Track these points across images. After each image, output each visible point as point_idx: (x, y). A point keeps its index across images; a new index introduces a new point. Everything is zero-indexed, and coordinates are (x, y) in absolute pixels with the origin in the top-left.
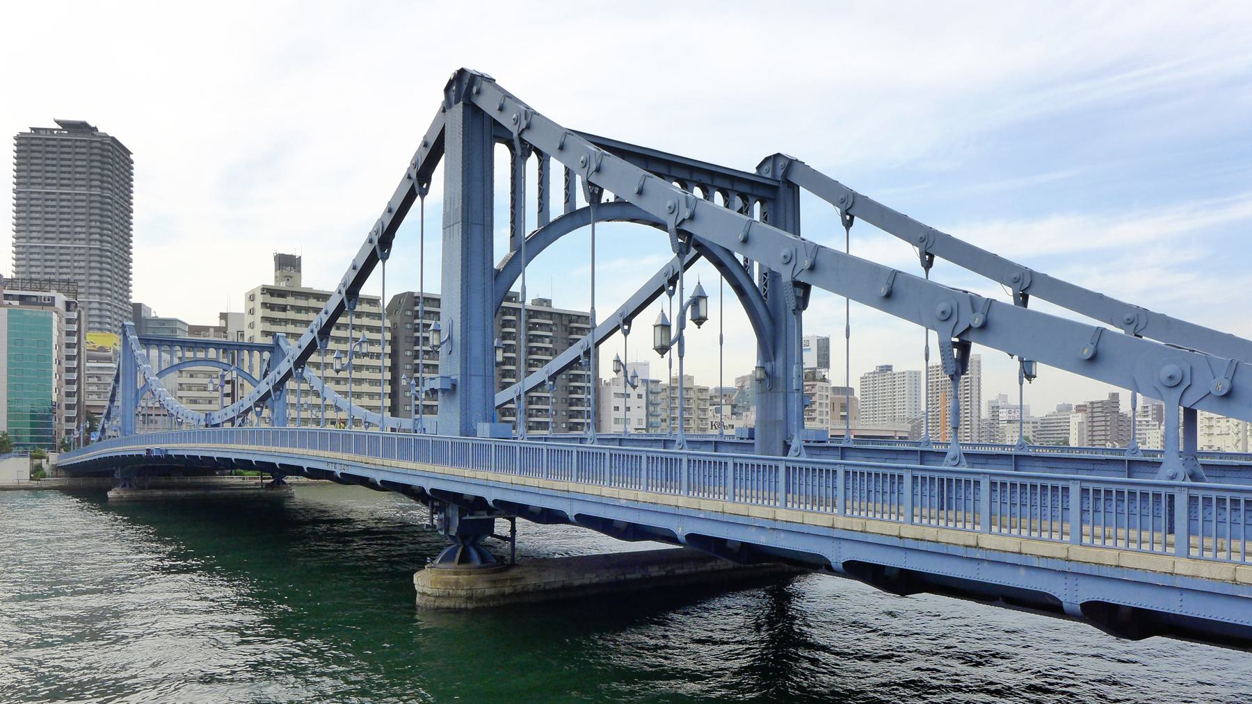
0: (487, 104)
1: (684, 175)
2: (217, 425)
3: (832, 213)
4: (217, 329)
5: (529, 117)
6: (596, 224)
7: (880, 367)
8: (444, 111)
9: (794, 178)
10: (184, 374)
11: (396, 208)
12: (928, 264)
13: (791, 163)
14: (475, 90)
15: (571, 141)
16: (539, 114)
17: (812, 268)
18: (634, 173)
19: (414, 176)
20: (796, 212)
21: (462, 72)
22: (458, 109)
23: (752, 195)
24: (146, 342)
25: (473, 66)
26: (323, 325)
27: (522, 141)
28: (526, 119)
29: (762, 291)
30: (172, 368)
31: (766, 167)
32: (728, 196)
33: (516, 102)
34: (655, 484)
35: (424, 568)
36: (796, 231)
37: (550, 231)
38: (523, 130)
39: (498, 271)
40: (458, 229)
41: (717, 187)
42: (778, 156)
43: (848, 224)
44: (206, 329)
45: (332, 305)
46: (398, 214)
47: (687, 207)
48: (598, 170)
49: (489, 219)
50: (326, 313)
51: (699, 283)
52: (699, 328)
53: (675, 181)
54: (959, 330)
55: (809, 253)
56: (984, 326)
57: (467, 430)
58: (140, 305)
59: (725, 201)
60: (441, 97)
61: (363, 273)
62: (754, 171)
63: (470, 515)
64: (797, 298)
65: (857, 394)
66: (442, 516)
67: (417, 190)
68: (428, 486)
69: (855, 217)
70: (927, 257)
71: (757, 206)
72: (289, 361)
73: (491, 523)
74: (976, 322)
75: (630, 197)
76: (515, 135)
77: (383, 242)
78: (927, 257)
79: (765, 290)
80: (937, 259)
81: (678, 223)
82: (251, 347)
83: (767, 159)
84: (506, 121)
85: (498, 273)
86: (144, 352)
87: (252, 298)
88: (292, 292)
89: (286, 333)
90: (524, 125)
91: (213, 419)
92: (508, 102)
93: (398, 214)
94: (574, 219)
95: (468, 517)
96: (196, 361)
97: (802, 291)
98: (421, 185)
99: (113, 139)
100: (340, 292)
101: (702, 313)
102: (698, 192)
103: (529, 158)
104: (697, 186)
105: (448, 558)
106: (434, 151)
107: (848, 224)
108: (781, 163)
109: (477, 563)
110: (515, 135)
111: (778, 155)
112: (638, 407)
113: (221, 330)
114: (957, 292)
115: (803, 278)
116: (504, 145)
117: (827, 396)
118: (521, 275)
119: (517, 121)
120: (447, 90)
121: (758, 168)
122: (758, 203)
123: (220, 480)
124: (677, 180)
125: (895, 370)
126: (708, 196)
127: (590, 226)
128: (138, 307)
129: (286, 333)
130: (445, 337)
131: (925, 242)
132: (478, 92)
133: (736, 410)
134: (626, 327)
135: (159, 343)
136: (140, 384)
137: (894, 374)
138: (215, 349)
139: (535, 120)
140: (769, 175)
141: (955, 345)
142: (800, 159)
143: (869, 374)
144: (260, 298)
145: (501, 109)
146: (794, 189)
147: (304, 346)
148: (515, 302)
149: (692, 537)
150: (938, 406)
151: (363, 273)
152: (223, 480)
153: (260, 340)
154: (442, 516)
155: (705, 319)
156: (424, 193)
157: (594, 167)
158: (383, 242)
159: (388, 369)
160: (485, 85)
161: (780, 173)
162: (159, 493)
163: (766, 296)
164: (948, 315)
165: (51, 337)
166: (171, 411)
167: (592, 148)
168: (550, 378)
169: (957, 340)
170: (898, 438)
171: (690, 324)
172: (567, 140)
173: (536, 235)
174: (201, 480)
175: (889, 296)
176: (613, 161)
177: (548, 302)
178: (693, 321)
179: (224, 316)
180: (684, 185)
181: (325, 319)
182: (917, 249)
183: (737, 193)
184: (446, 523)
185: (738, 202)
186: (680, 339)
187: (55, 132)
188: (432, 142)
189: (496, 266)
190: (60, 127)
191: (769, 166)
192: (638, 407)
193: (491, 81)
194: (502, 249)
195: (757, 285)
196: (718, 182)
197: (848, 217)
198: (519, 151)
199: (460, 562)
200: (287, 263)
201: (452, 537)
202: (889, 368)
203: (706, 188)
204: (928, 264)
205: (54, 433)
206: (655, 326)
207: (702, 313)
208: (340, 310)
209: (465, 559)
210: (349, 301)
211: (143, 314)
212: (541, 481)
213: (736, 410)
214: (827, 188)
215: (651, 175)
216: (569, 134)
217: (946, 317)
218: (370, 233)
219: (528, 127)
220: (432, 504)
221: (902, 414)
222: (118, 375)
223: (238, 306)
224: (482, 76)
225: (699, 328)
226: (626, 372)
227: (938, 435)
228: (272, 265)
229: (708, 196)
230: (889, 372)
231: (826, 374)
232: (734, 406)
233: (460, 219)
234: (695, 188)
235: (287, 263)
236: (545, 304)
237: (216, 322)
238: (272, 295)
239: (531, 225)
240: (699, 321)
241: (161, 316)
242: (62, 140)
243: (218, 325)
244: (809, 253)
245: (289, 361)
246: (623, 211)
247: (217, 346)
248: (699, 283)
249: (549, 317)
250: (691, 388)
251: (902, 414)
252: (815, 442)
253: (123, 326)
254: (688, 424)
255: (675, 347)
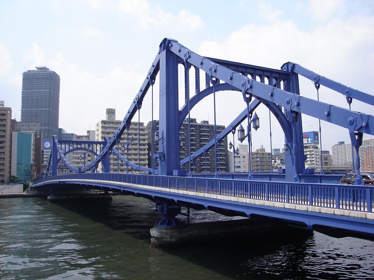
0: (174, 50)
1: (244, 70)
2: (83, 172)
3: (311, 84)
4: (86, 136)
5: (190, 54)
6: (215, 93)
7: (339, 142)
8: (159, 54)
9: (296, 71)
10: (75, 153)
11: (143, 89)
12: (350, 102)
13: (294, 65)
14: (170, 45)
15: (206, 61)
16: (193, 52)
17: (298, 105)
18: (229, 72)
19: (149, 78)
20: (297, 83)
21: (165, 39)
22: (164, 52)
23: (272, 76)
24: (61, 142)
25: (169, 37)
26: (118, 134)
27: (187, 62)
28: (188, 54)
29: (285, 115)
30: (70, 151)
31: (284, 67)
32: (270, 79)
33: (185, 49)
34: (243, 193)
35: (154, 227)
36: (298, 93)
37: (200, 95)
38: (188, 58)
39: (180, 112)
40: (165, 96)
41: (248, 73)
42: (288, 63)
43: (318, 88)
44: (82, 136)
45: (121, 126)
46: (144, 92)
47: (249, 84)
48: (215, 71)
49: (177, 92)
50: (119, 129)
51: (255, 113)
52: (256, 130)
53: (240, 73)
54: (357, 128)
55: (296, 100)
56: (367, 126)
57: (170, 173)
58: (61, 129)
59: (261, 79)
60: (158, 48)
61: (132, 114)
62: (280, 69)
63: (171, 206)
64: (293, 117)
65: (331, 153)
66: (161, 206)
67: (151, 83)
68: (153, 195)
69: (320, 85)
70: (349, 99)
71: (282, 82)
72: (107, 148)
73: (180, 209)
74: (364, 125)
75: (229, 82)
76: (185, 60)
77: (138, 103)
78: (349, 99)
79: (287, 114)
80: (353, 99)
81: (245, 90)
82: (97, 143)
83: (284, 64)
84: (182, 55)
85: (180, 112)
86: (60, 146)
87: (98, 125)
88: (112, 122)
89: (109, 137)
90: (188, 57)
91: (81, 170)
92: (182, 49)
93: (144, 92)
94: (208, 91)
95: (170, 207)
96: (77, 149)
97: (295, 115)
98: (152, 81)
99: (54, 72)
100: (124, 122)
101: (257, 125)
102: (249, 76)
103: (190, 69)
104: (266, 77)
105: (162, 223)
106: (156, 68)
107: (318, 88)
108: (290, 66)
109: (174, 224)
110: (185, 60)
111: (289, 62)
112: (244, 161)
113: (88, 137)
114: (356, 113)
115: (295, 109)
116: (182, 65)
117: (318, 155)
118: (188, 114)
119: (185, 55)
120: (160, 46)
121: (281, 68)
122: (282, 81)
123: (86, 192)
124: (250, 74)
125: (345, 143)
126: (254, 78)
127: (213, 94)
128: (61, 130)
129: (109, 137)
130: (160, 137)
131: (348, 93)
132: (171, 46)
133: (282, 161)
134: (234, 131)
135: (65, 142)
136: (59, 157)
137: (345, 145)
138: (72, 144)
139: (192, 54)
140: (286, 70)
141: (356, 134)
142: (297, 64)
143: (335, 145)
144: (100, 125)
145: (180, 51)
146: (296, 75)
147: (112, 142)
148: (195, 122)
149: (252, 215)
150: (363, 157)
151: (132, 114)
152: (88, 192)
153: (100, 140)
154: (161, 206)
155: (259, 127)
156: (153, 83)
157: (213, 70)
158: (138, 103)
159: (147, 149)
160: (174, 43)
161: (290, 69)
162: (71, 197)
163: (287, 117)
164: (352, 123)
165: (31, 142)
166: (68, 167)
167: (213, 63)
168: (205, 152)
169: (357, 132)
170: (348, 170)
171: (253, 129)
172: (204, 61)
173: (194, 98)
174: (80, 192)
175: (329, 115)
176: (220, 68)
177: (207, 122)
178: (254, 128)
179: (88, 132)
180: (243, 74)
181: (119, 132)
182: (345, 96)
183: (273, 78)
184: (162, 209)
185: (274, 81)
186: (249, 135)
187: (36, 71)
188: (155, 65)
189: (180, 109)
190: (37, 69)
191: (285, 67)
192: (244, 161)
193: (176, 42)
194: (182, 104)
195: (283, 112)
196: (266, 73)
197: (317, 85)
198: (186, 67)
199: (168, 225)
200: (111, 112)
201: (164, 215)
202: (343, 143)
203: (269, 77)
204: (350, 102)
205: (31, 175)
206: (238, 131)
207: (257, 125)
208: (124, 128)
209: (169, 223)
210: (127, 125)
211: (63, 132)
212: (194, 193)
213: (282, 161)
214: (310, 75)
215: (235, 72)
216: (204, 59)
217: (351, 123)
218: (134, 99)
219: (189, 57)
220: (157, 202)
221: (349, 161)
222: (51, 154)
223: (93, 128)
224: (173, 40)
225: (256, 130)
226: (234, 148)
227: (364, 169)
228: (105, 112)
229: (254, 78)
230: (343, 144)
231: (318, 146)
232: (281, 160)
233: (165, 93)
234: (273, 79)
235: (111, 112)
236: (206, 123)
237: (86, 134)
238: (105, 123)
239: (193, 93)
240: (256, 127)
241: (68, 132)
242: (38, 74)
243: (87, 135)
244: (296, 100)
245: (107, 148)
246: (227, 87)
247: (85, 143)
248: (255, 113)
249: (207, 128)
250: (264, 153)
251: (349, 161)
252: (309, 174)
253: (53, 137)
254: (264, 167)
255: (247, 139)
